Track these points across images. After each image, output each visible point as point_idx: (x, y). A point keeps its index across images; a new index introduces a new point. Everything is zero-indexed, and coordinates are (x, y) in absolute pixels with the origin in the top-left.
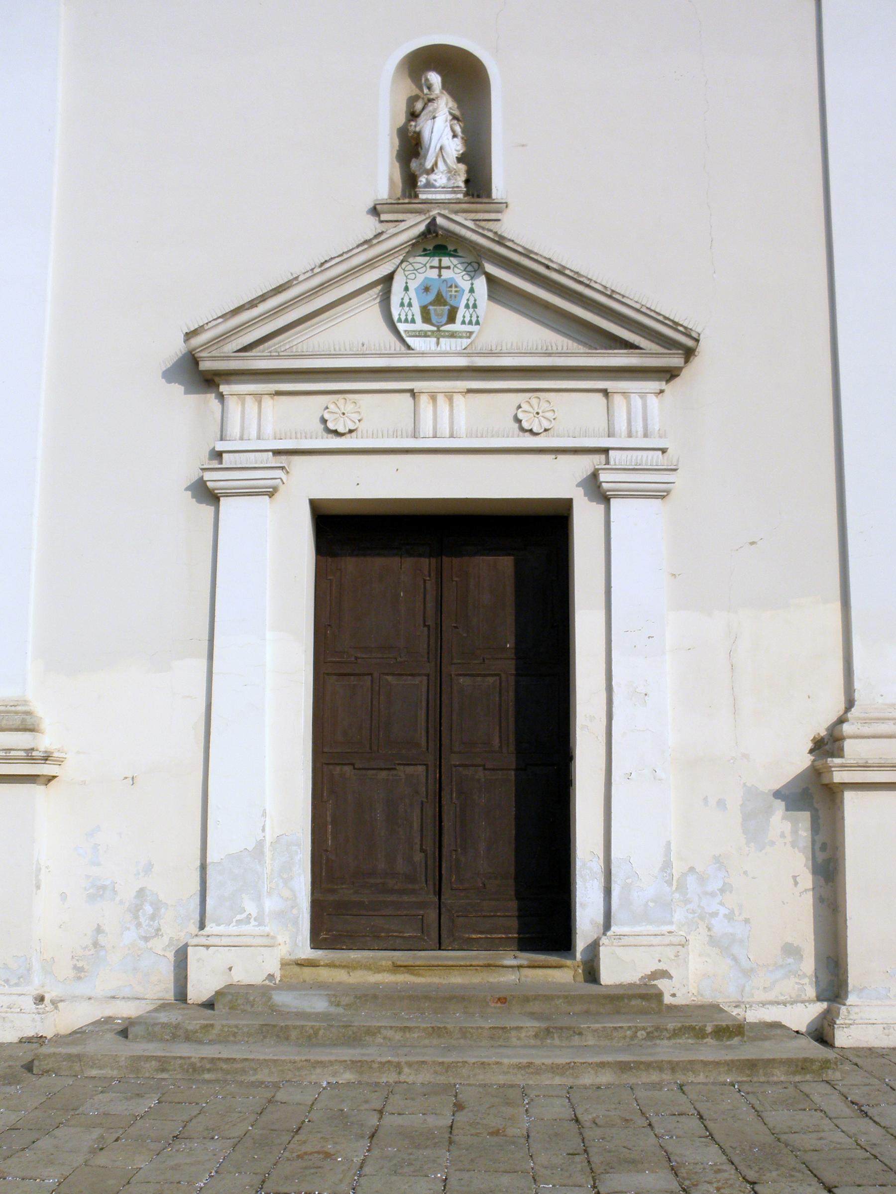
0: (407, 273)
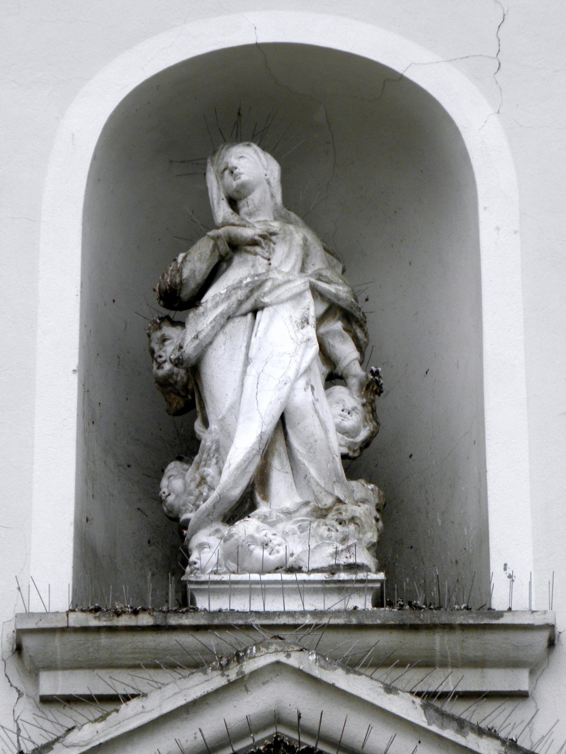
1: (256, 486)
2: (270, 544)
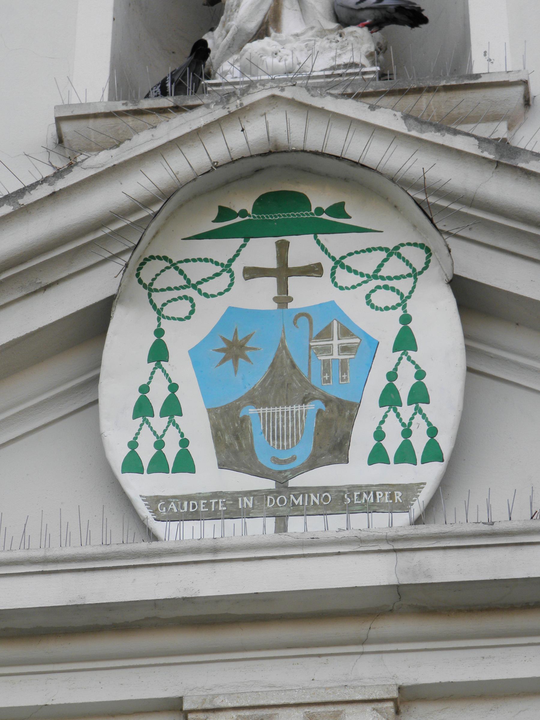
0: (159, 299)
1: (270, 23)
2: (279, 54)
